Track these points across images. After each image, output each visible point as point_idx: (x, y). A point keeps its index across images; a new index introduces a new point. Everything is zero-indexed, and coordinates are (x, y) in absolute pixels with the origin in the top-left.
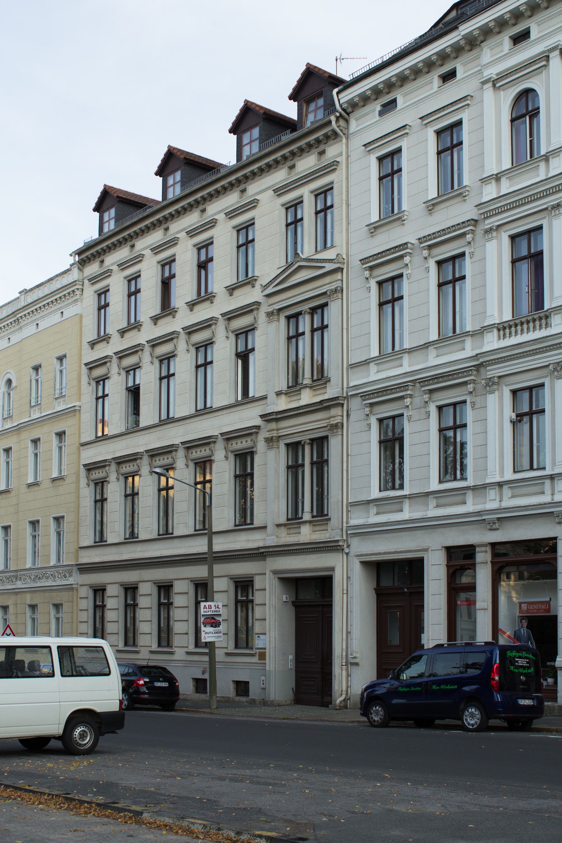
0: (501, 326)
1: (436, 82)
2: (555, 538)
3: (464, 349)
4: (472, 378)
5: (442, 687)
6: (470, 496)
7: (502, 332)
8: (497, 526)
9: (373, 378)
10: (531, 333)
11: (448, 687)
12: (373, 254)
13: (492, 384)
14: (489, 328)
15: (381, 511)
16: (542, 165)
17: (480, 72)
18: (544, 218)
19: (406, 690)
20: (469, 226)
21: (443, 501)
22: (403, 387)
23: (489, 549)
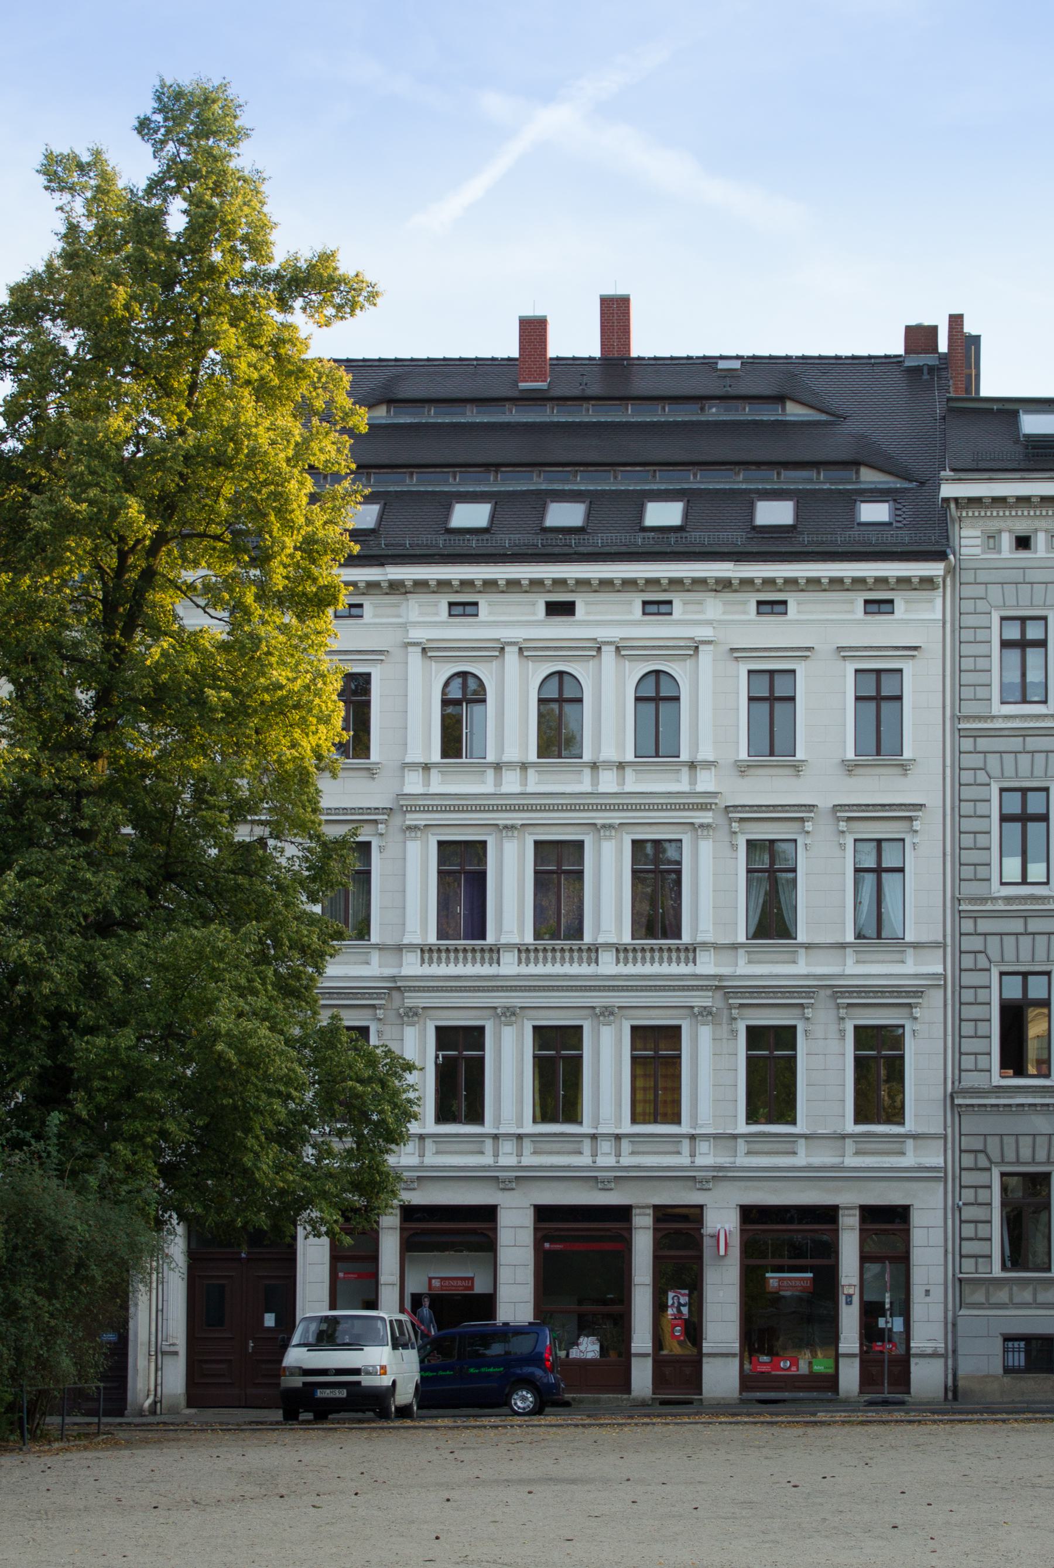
0: (524, 948)
1: (542, 609)
2: (701, 1207)
3: (368, 963)
4: (383, 1002)
5: (483, 1370)
6: (801, 1145)
7: (426, 955)
8: (711, 1185)
9: (740, 971)
10: (549, 965)
11: (491, 1370)
12: (742, 803)
13: (412, 1014)
14: (411, 947)
15: (636, 1150)
16: (490, 773)
17: (404, 626)
18: (588, 834)
19: (431, 1374)
20: (383, 814)
21: (443, 1147)
22: (809, 992)
23: (650, 1211)
